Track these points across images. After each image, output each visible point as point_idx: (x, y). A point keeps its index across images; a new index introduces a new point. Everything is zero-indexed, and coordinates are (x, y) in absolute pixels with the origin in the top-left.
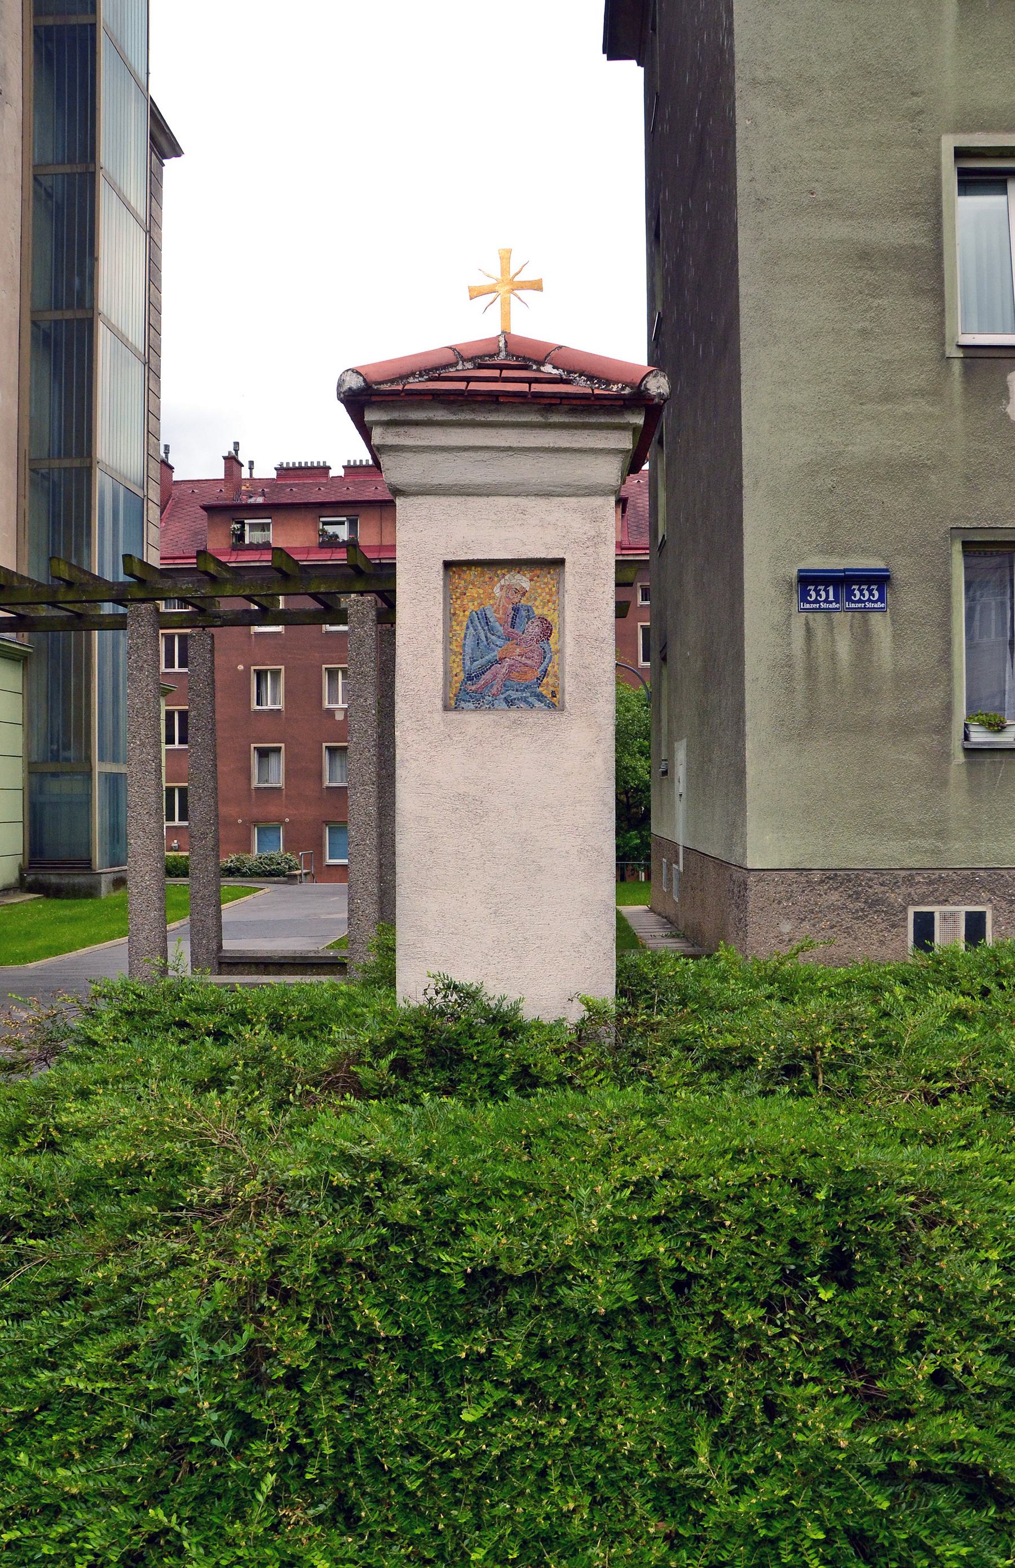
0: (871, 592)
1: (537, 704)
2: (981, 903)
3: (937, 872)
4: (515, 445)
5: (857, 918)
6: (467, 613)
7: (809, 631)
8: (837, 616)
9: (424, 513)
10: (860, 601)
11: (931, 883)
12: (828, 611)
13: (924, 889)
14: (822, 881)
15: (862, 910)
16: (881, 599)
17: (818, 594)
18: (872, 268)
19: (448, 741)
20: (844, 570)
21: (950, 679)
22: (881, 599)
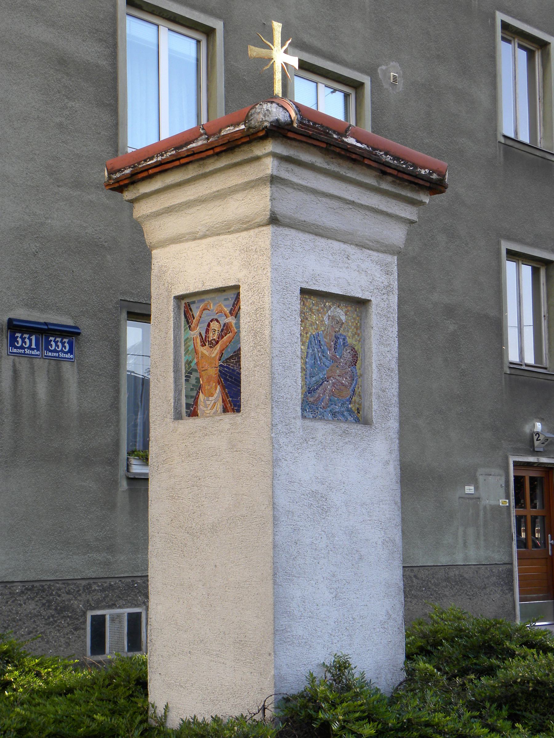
0: (63, 344)
1: (350, 418)
2: (137, 606)
3: (108, 581)
4: (357, 201)
5: (48, 624)
6: (308, 335)
7: (15, 372)
8: (38, 362)
9: (288, 243)
10: (55, 351)
11: (103, 590)
12: (31, 357)
13: (99, 596)
14: (22, 592)
15: (53, 616)
16: (71, 351)
17: (24, 341)
18: (68, 74)
19: (305, 445)
20: (46, 324)
21: (118, 421)
22: (71, 351)
